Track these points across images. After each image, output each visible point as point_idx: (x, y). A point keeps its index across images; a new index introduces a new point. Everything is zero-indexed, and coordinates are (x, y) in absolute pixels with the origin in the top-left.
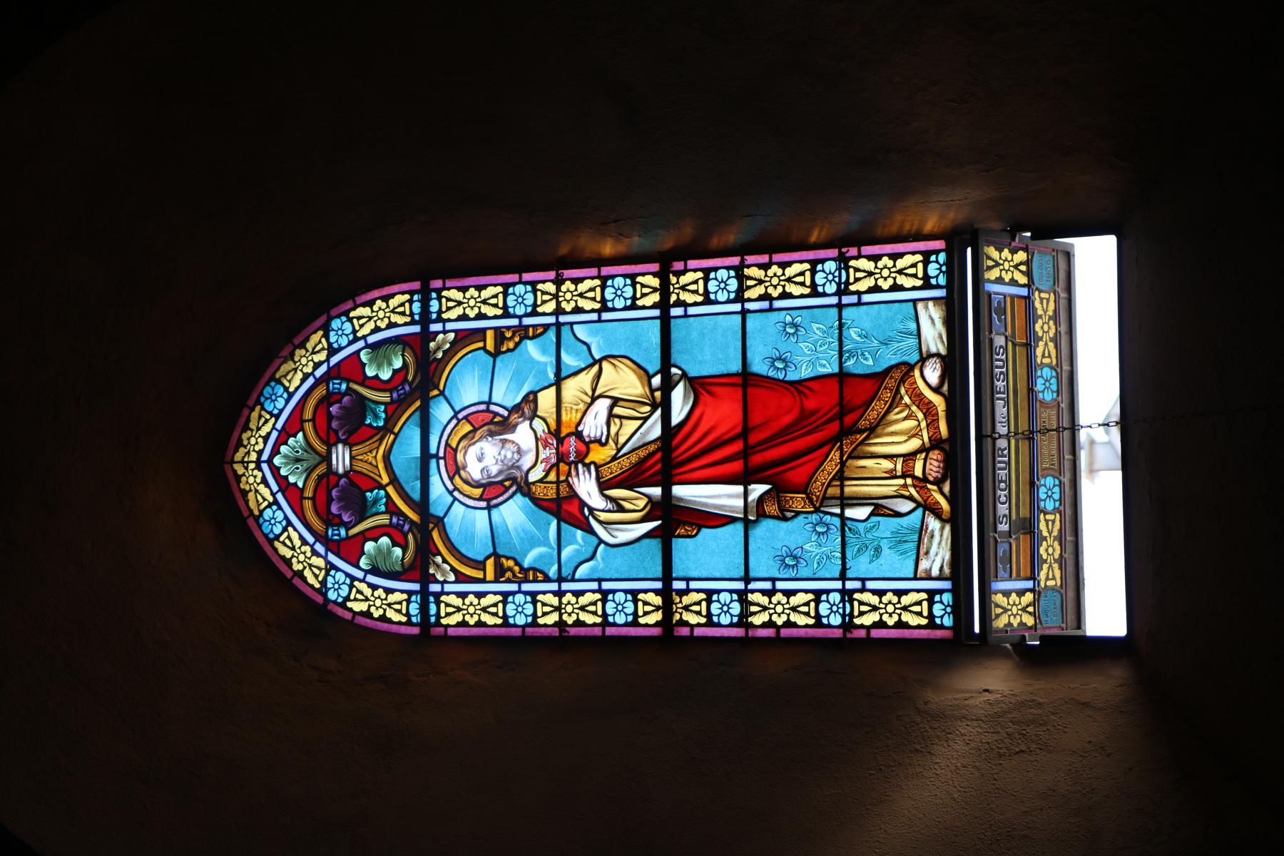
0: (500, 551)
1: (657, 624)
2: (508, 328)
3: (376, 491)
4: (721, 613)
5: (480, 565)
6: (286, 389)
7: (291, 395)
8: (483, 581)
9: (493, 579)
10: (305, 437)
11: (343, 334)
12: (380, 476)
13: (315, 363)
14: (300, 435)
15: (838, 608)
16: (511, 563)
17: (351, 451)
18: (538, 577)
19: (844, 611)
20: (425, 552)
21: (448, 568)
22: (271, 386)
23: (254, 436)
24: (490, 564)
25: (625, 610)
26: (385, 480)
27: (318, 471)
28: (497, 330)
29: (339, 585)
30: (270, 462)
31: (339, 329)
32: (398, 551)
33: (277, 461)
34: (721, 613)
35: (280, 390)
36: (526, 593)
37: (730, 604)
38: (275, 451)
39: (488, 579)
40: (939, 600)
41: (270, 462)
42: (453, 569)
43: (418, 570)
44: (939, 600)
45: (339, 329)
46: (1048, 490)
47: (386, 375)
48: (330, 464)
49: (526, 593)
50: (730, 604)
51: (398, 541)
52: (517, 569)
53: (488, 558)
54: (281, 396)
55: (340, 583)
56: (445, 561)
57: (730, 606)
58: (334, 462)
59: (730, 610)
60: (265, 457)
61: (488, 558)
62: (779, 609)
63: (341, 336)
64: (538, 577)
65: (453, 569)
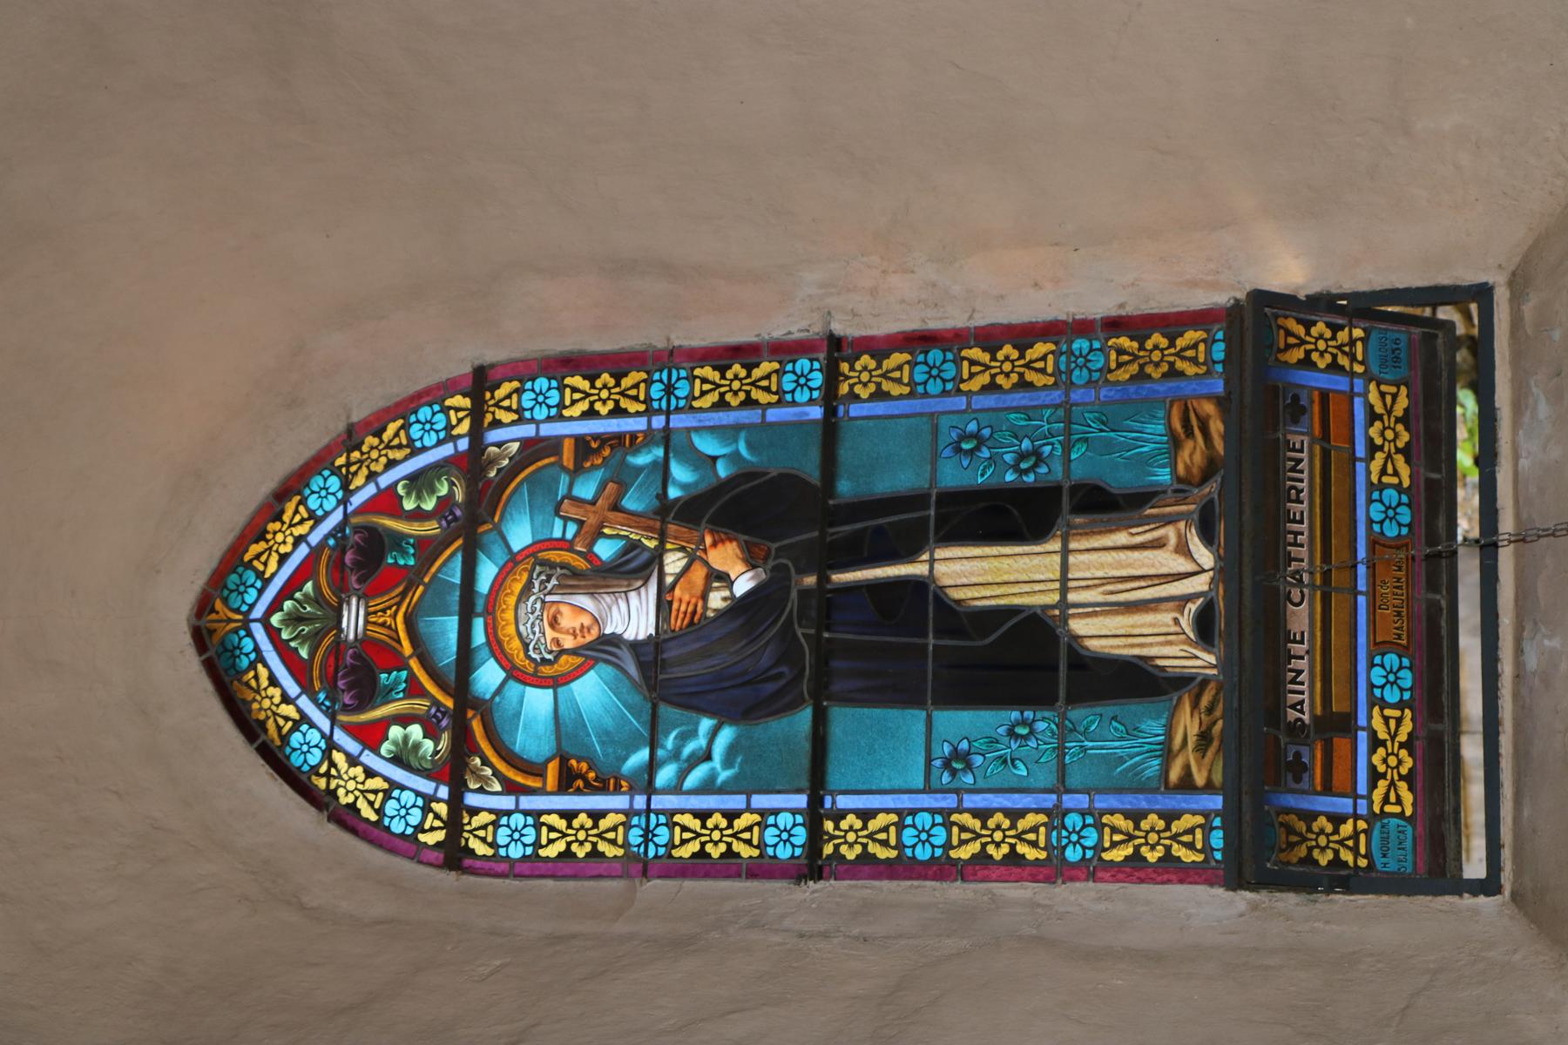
0: (566, 747)
1: (438, 844)
2: (596, 437)
3: (395, 673)
4: (778, 843)
5: (537, 770)
6: (259, 575)
7: (267, 582)
8: (541, 791)
9: (555, 789)
10: (317, 587)
11: (432, 429)
12: (399, 641)
13: (389, 460)
14: (309, 587)
15: (1068, 837)
16: (584, 766)
17: (367, 607)
18: (621, 787)
19: (1059, 834)
20: (463, 746)
21: (489, 772)
22: (323, 476)
23: (380, 451)
24: (552, 770)
25: (916, 833)
26: (407, 648)
27: (327, 642)
28: (581, 442)
29: (1395, 674)
30: (265, 621)
31: (427, 422)
32: (429, 745)
33: (275, 620)
34: (778, 843)
35: (250, 577)
36: (526, 813)
37: (930, 829)
38: (275, 606)
39: (549, 788)
40: (911, 823)
41: (265, 621)
42: (496, 773)
43: (453, 772)
44: (911, 823)
45: (427, 422)
46: (1388, 673)
47: (429, 505)
48: (340, 630)
49: (526, 813)
50: (930, 829)
51: (431, 732)
52: (592, 775)
53: (549, 760)
54: (252, 586)
55: (1395, 670)
56: (485, 762)
57: (792, 832)
58: (344, 625)
59: (510, 833)
60: (258, 612)
61: (549, 760)
62: (851, 837)
63: (428, 431)
64: (621, 787)
65: (496, 773)
